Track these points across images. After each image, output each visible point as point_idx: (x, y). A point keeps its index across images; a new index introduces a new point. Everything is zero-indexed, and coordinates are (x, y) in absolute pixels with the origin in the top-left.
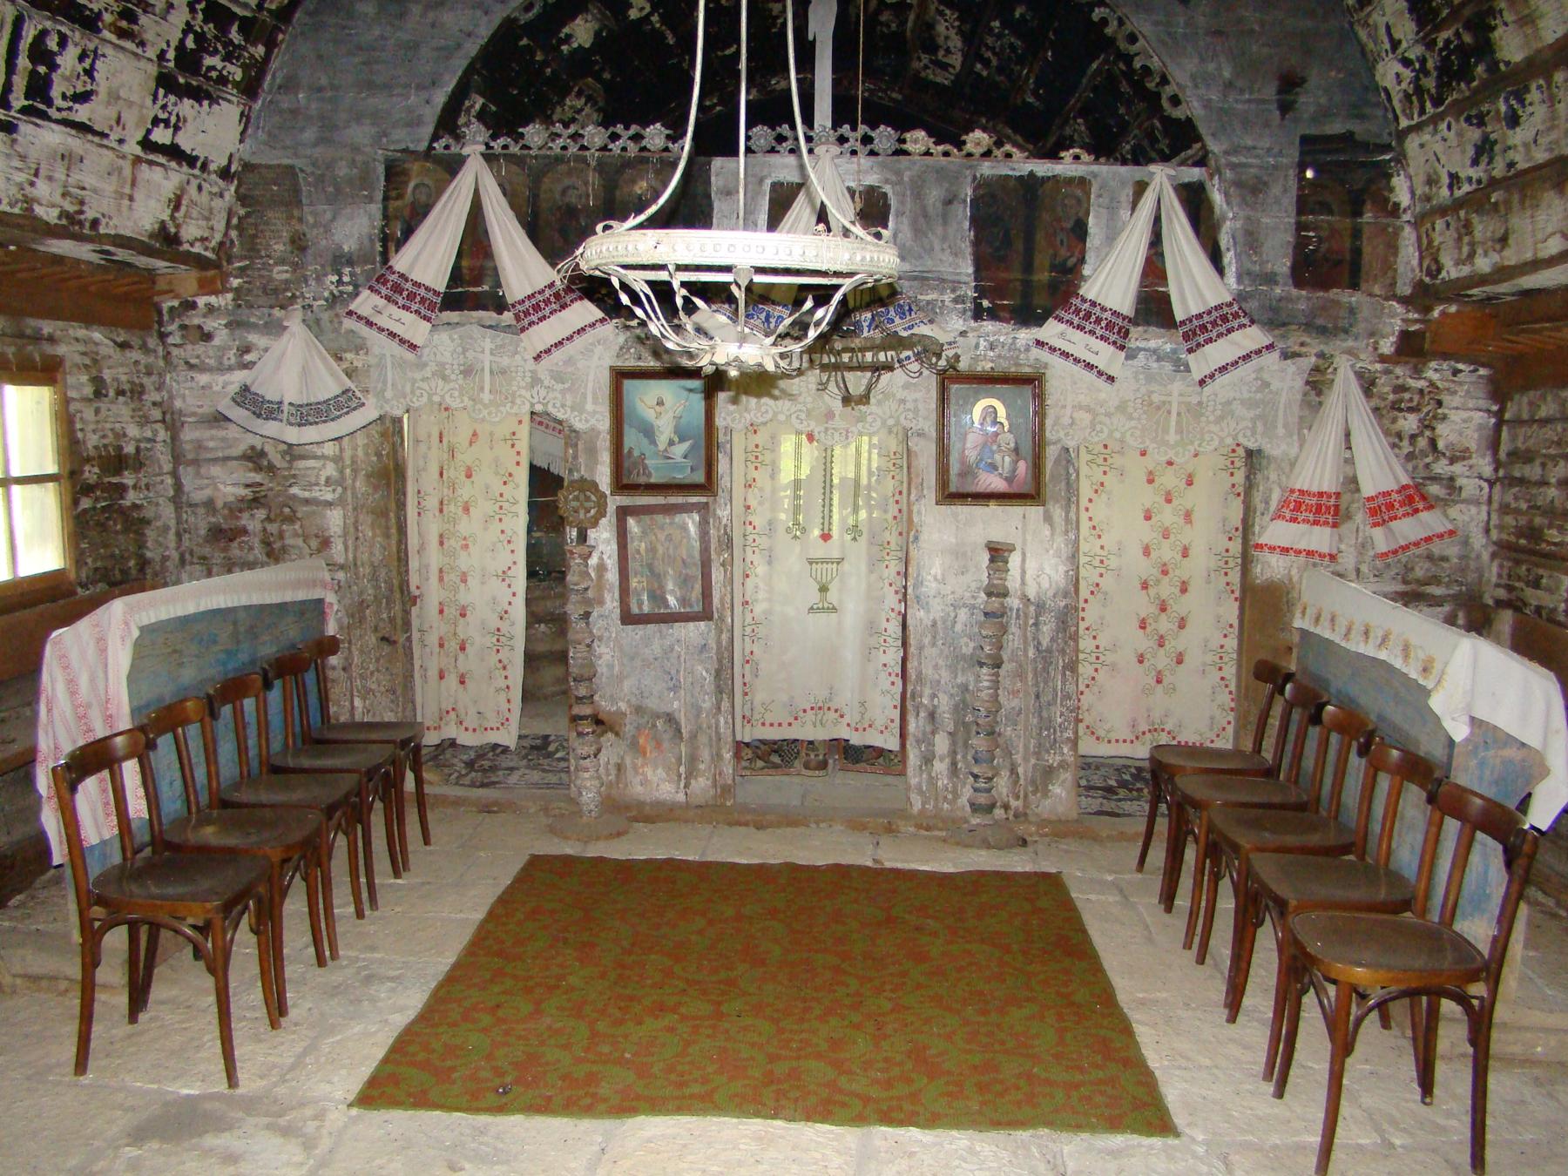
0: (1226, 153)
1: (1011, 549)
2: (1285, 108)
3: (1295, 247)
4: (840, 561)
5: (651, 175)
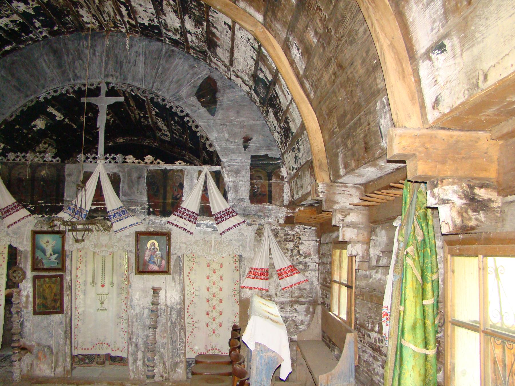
0: (227, 162)
1: (160, 289)
2: (245, 147)
3: (250, 191)
4: (107, 294)
5: (47, 169)
